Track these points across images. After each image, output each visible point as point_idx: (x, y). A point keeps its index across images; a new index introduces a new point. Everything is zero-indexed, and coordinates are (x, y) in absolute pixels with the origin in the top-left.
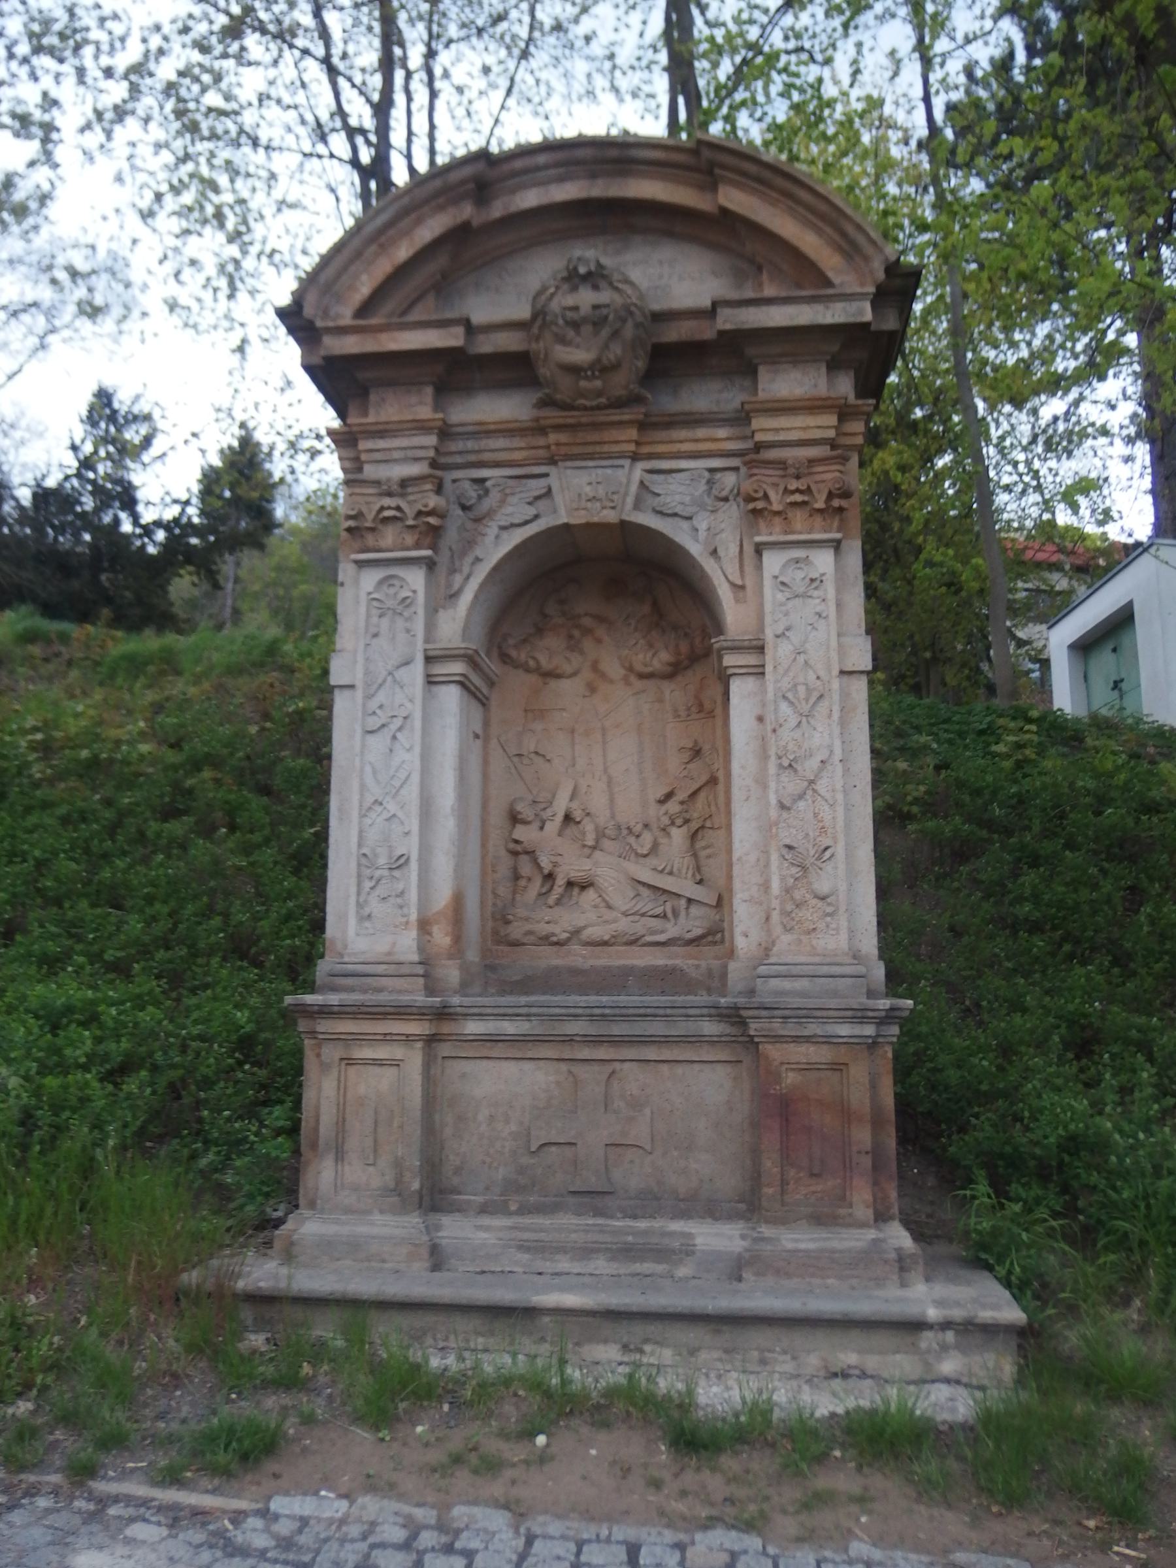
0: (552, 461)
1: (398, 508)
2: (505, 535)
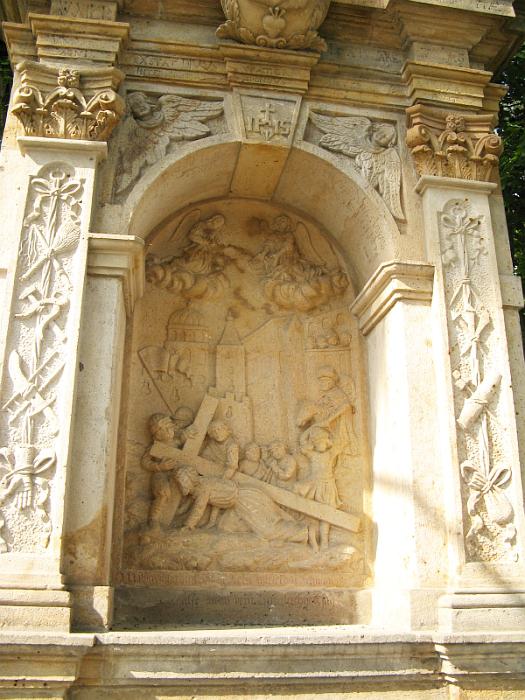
0: (227, 88)
1: (74, 99)
2: (175, 146)
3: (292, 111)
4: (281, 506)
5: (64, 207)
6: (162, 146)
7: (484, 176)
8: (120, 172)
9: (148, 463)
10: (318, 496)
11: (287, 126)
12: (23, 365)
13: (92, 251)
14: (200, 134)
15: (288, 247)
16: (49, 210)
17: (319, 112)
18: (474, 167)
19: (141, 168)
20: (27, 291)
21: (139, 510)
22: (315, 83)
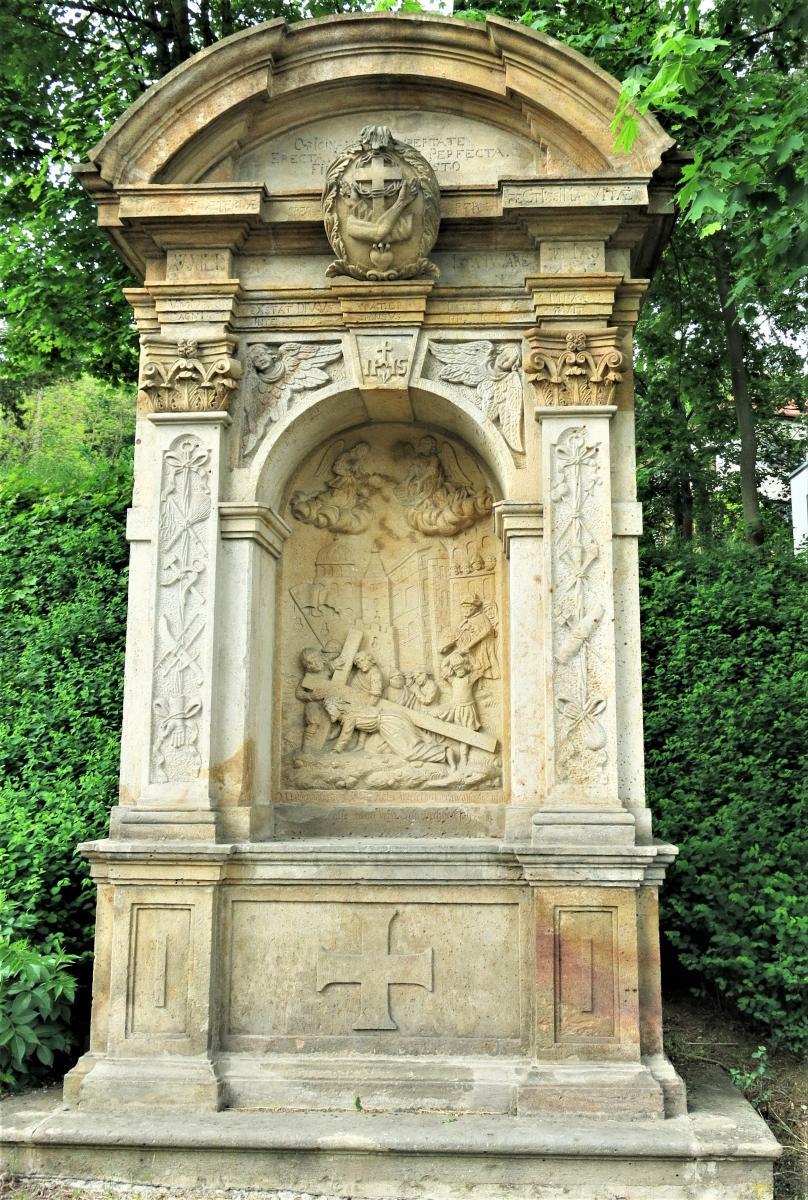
0: (344, 329)
1: (195, 370)
2: (298, 397)
3: (407, 344)
4: (422, 729)
5: (194, 475)
6: (284, 401)
7: (606, 398)
8: (247, 432)
9: (302, 693)
10: (456, 719)
11: (404, 364)
12: (169, 626)
13: (223, 517)
14: (320, 382)
15: (432, 470)
16: (182, 479)
17: (438, 341)
18: (594, 389)
19: (267, 425)
20: (168, 560)
21: (294, 735)
22: (432, 311)
